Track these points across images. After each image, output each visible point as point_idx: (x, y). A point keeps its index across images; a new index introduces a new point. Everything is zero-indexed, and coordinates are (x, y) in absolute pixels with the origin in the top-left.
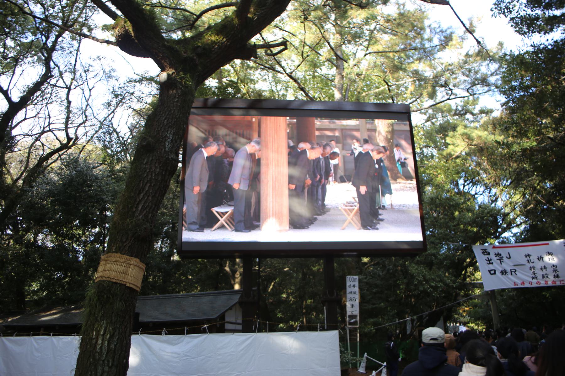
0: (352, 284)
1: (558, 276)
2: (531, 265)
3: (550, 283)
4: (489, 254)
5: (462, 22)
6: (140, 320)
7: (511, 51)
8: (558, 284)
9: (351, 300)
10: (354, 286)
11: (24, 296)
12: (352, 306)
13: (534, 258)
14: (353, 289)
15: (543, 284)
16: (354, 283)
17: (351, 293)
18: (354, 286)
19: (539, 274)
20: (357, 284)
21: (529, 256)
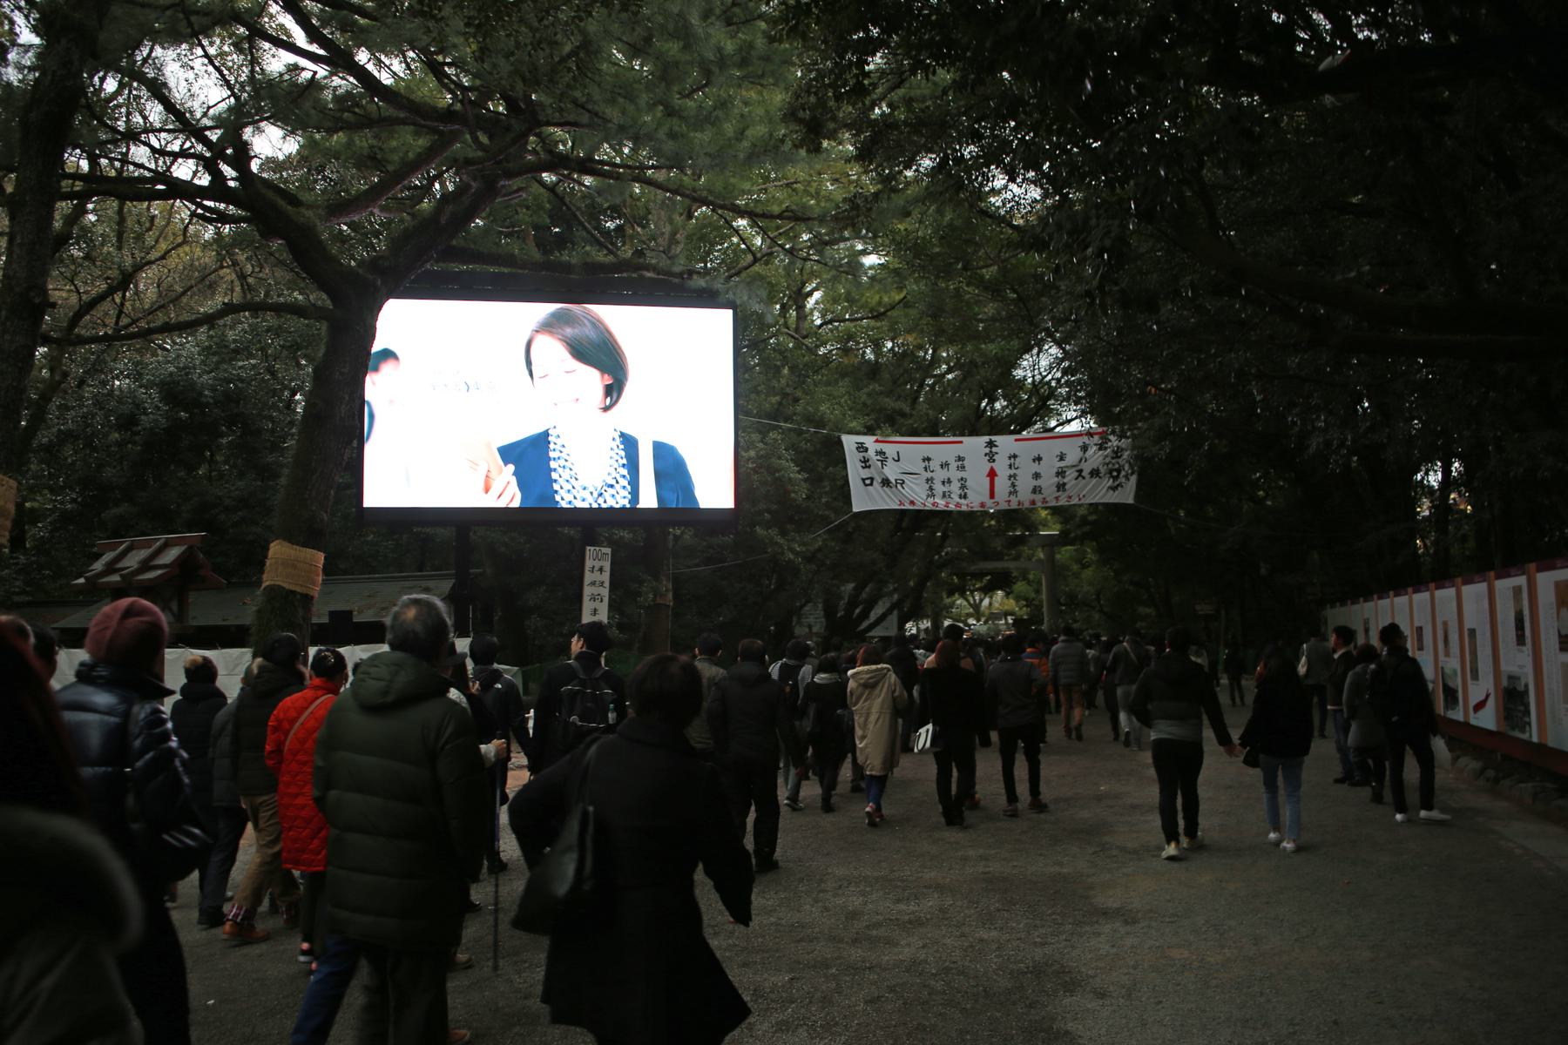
0: (597, 564)
1: (965, 497)
2: (929, 475)
3: (952, 507)
4: (866, 450)
5: (529, 363)
6: (400, 322)
7: (1337, 781)
8: (964, 508)
9: (593, 599)
10: (601, 570)
11: (455, 112)
12: (595, 612)
13: (935, 465)
14: (597, 576)
15: (941, 504)
16: (601, 563)
17: (593, 583)
18: (601, 570)
19: (939, 489)
20: (607, 565)
21: (929, 459)
